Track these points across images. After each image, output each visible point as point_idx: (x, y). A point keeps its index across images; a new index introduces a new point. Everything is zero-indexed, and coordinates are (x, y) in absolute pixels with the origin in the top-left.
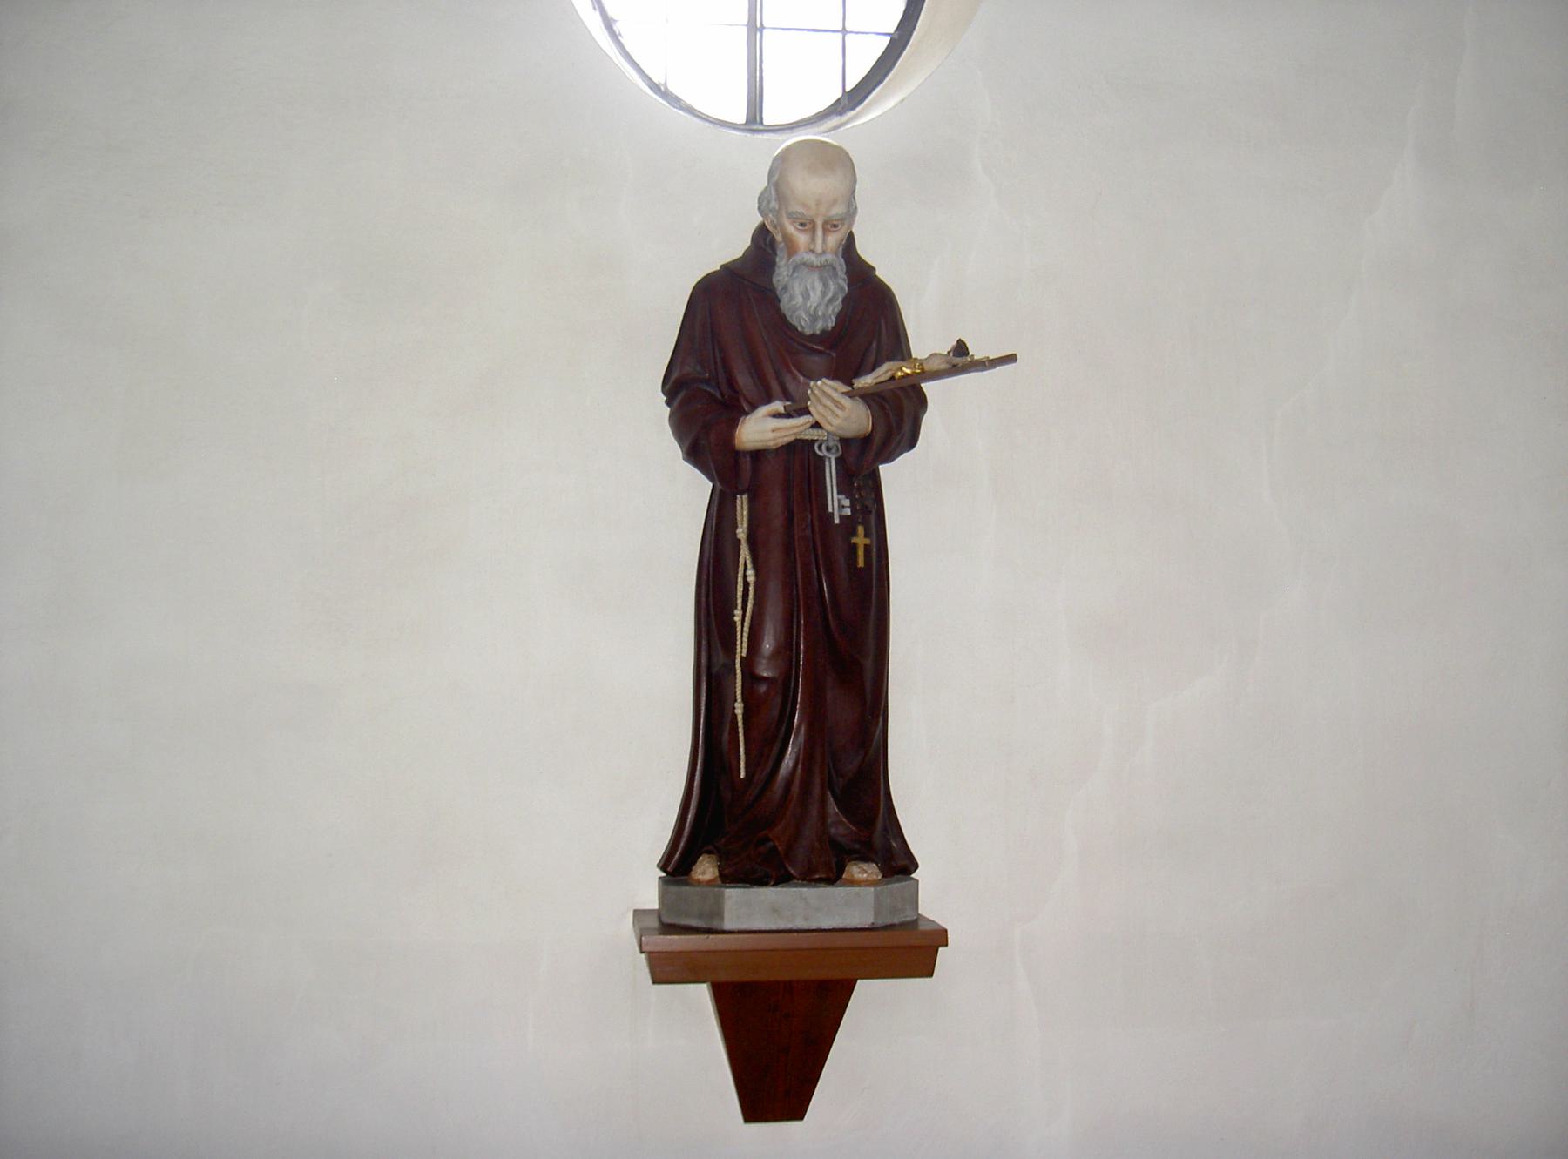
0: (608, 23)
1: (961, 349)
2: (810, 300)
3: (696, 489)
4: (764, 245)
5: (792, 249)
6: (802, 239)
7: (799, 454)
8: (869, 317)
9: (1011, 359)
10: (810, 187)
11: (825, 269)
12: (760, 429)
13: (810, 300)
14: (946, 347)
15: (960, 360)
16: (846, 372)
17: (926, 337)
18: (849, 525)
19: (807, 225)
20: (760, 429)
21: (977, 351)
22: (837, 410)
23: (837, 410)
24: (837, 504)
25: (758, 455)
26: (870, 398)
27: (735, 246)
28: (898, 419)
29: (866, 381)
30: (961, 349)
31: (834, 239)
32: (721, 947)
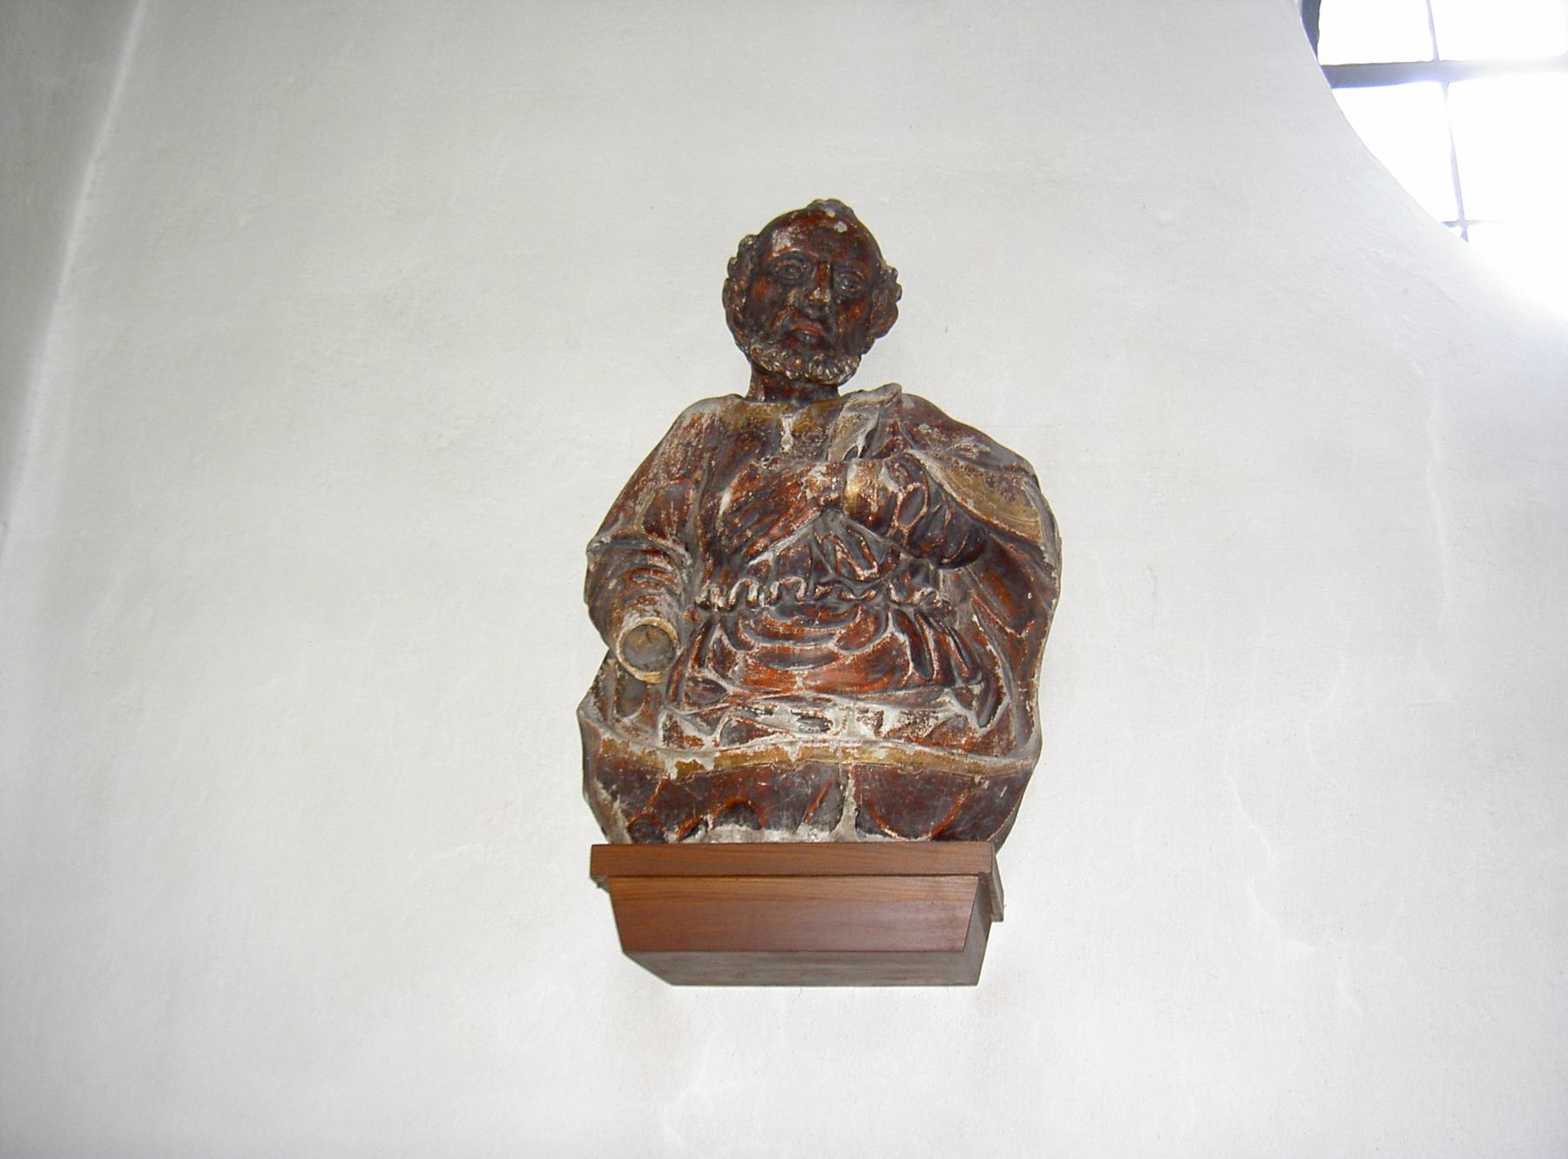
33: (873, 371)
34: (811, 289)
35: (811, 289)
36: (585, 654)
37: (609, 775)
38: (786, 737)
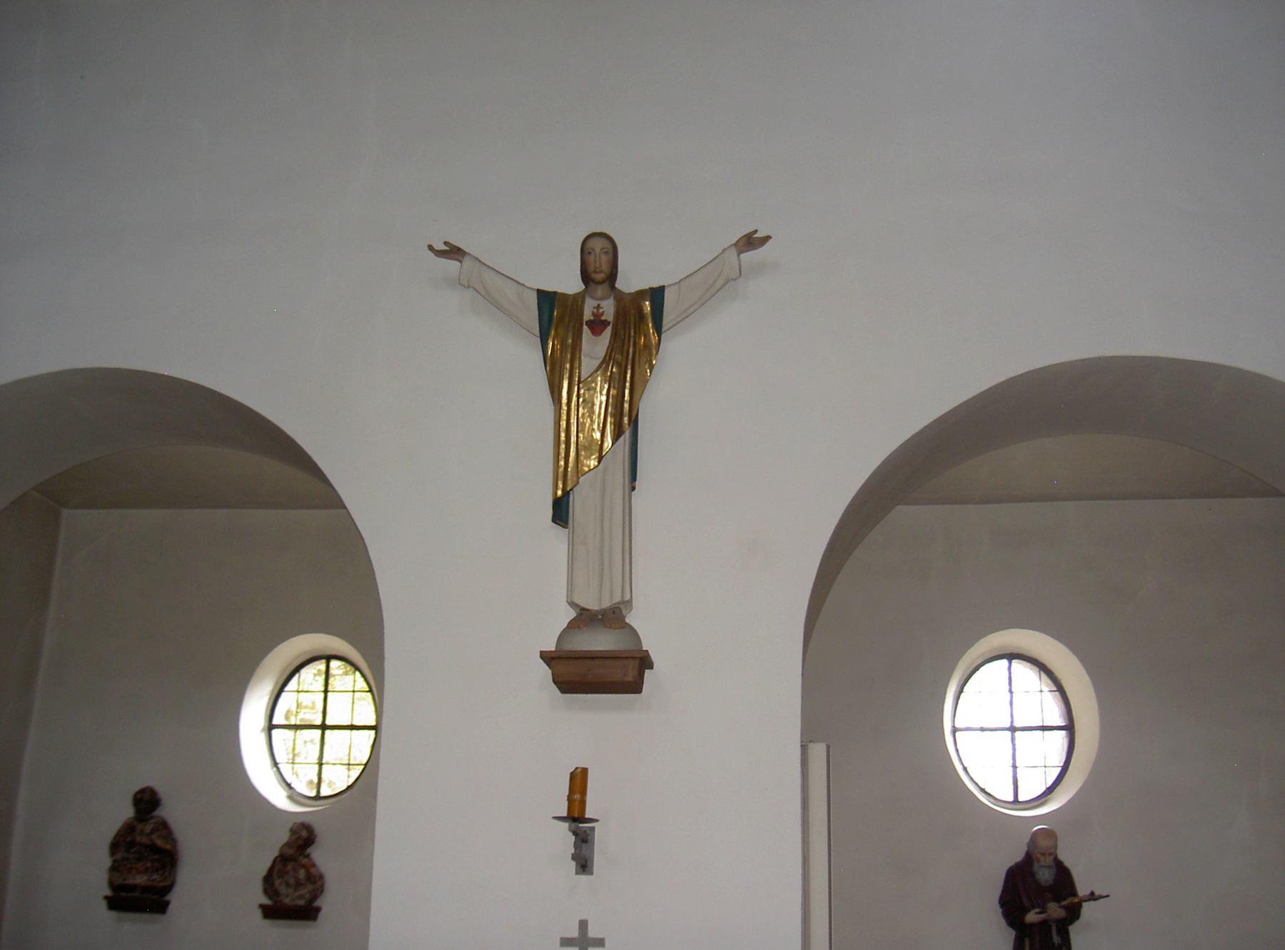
0: (965, 769)
1: (1092, 893)
2: (1045, 875)
3: (1011, 934)
4: (1029, 859)
5: (1039, 861)
6: (1042, 858)
7: (1044, 923)
8: (1063, 880)
9: (584, 865)
10: (1043, 843)
11: (1049, 867)
12: (1032, 917)
13: (1045, 875)
14: (1088, 893)
15: (1092, 897)
16: (1058, 899)
17: (1082, 890)
18: (1060, 946)
19: (1043, 854)
20: (1032, 917)
21: (1097, 893)
22: (1055, 910)
23: (1055, 910)
24: (1056, 939)
25: (1032, 925)
26: (1065, 908)
27: (1018, 856)
28: (1074, 913)
29: (1064, 903)
30: (1092, 893)
31: (1049, 860)
32: (1093, 704)
33: (156, 813)
34: (147, 802)
35: (147, 802)
36: (107, 862)
37: (112, 885)
38: (130, 881)
